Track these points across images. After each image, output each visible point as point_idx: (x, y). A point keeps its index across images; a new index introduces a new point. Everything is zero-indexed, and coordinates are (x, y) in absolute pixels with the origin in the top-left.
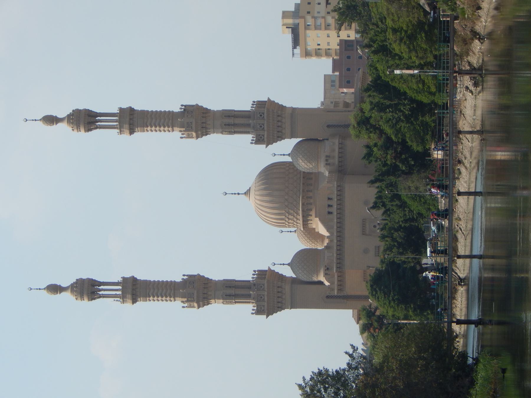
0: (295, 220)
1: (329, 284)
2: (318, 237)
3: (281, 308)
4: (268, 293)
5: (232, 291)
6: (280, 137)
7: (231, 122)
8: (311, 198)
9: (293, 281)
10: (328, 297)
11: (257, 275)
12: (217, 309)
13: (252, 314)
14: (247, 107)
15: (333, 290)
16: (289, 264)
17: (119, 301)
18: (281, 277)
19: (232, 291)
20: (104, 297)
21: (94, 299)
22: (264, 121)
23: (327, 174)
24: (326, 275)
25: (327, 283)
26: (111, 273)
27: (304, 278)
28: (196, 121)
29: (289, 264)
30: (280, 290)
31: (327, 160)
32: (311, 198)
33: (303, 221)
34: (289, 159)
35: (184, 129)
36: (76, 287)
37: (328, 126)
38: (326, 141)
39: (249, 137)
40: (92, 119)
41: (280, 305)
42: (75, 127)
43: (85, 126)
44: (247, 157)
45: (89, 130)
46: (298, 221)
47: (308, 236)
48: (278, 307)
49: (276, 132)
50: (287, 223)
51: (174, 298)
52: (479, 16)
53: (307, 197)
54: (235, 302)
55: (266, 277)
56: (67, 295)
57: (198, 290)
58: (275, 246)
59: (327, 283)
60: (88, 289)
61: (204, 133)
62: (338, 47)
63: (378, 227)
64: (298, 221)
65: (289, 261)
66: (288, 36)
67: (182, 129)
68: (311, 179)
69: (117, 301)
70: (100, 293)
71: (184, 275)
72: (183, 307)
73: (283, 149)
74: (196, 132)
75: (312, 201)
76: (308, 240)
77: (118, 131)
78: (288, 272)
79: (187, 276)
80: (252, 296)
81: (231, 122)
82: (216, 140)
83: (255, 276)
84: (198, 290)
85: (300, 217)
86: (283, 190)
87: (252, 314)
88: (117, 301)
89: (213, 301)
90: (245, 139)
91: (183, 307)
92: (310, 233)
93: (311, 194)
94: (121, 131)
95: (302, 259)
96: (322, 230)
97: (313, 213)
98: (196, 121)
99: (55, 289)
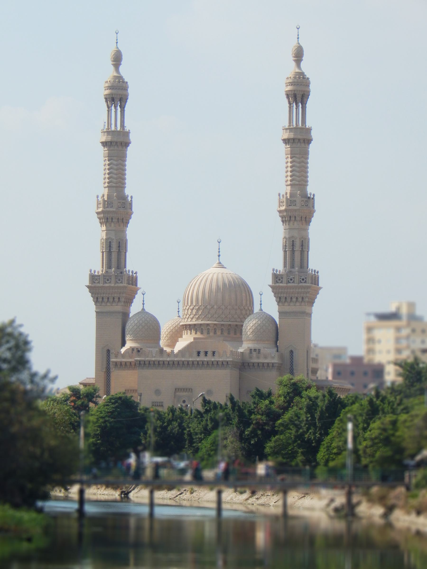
0: (191, 316)
1: (122, 353)
3: (96, 301)
4: (113, 288)
5: (115, 250)
6: (280, 300)
7: (297, 249)
8: (215, 333)
9: (125, 315)
10: (108, 351)
11: (132, 275)
12: (98, 233)
13: (91, 271)
15: (116, 357)
16: (143, 309)
17: (104, 128)
18: (129, 301)
19: (115, 250)
20: (108, 111)
21: (106, 101)
22: (297, 284)
23: (241, 350)
24: (133, 349)
25: (123, 350)
27: (129, 326)
28: (298, 211)
29: (143, 309)
30: (116, 300)
31: (255, 350)
32: (215, 333)
33: (190, 325)
34: (256, 309)
35: (289, 197)
36: (119, 82)
37: (292, 352)
38: (275, 349)
40: (299, 99)
41: (100, 300)
42: (290, 81)
43: (292, 90)
44: (258, 265)
45: (288, 96)
46: (189, 320)
47: (174, 330)
48: (97, 298)
49: (285, 295)
50: (187, 308)
51: (108, 187)
53: (215, 329)
54: (103, 252)
57: (116, 213)
58: (166, 297)
59: (123, 350)
61: (284, 219)
64: (189, 320)
67: (288, 196)
68: (235, 333)
69: (105, 126)
70: (113, 108)
71: (132, 197)
72: (98, 197)
73: (267, 304)
74: (286, 210)
75: (212, 334)
76: (169, 330)
77: (287, 127)
78: (135, 309)
79: (131, 200)
80: (109, 270)
81: (297, 249)
82: (277, 232)
83: (131, 274)
84: (116, 213)
85: (194, 322)
87: (91, 271)
88: (105, 126)
89: (104, 228)
91: (98, 197)
93: (219, 333)
94: (286, 129)
95: (150, 328)
97: (199, 335)
98: (298, 211)
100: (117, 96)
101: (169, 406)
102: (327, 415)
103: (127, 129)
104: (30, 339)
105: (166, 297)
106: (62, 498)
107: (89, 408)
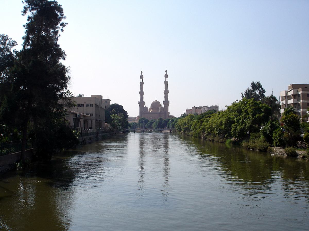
2: (150, 110)
3: (164, 105)
4: (142, 103)
5: (142, 98)
7: (166, 97)
12: (139, 96)
14: (168, 100)
19: (142, 98)
22: (166, 102)
26: (169, 80)
27: (144, 109)
28: (166, 92)
34: (161, 106)
39: (140, 101)
44: (161, 100)
57: (142, 93)
58: (148, 105)
63: (171, 149)
66: (23, 9)
73: (162, 105)
78: (145, 106)
81: (166, 97)
82: (163, 95)
84: (142, 93)
86: (156, 104)
90: (164, 99)
92: (150, 109)
95: (146, 108)
96: (151, 111)
98: (166, 92)
99: (166, 71)
100: (142, 77)
101: (217, 107)
102: (52, 131)
104: (63, 9)
105: (148, 105)
106: (137, 122)
107: (139, 121)
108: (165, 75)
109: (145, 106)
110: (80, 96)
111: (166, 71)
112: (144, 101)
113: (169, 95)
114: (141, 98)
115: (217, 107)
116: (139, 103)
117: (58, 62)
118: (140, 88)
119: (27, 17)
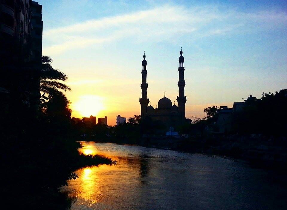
4: (144, 101)
5: (144, 93)
7: (182, 91)
12: (140, 90)
19: (144, 93)
22: (182, 99)
26: (148, 68)
28: (181, 84)
39: (141, 98)
52: (84, 199)
55: (147, 101)
56: (143, 59)
57: (144, 86)
58: (154, 103)
60: (144, 63)
62: (275, 94)
65: (151, 105)
78: (149, 105)
81: (182, 91)
84: (144, 86)
86: (164, 102)
95: (151, 107)
98: (181, 84)
99: (144, 56)
103: (146, 70)
105: (154, 103)
108: (142, 62)
109: (149, 105)
110: (235, 104)
111: (144, 56)
112: (147, 97)
113: (148, 90)
114: (145, 93)
115: (227, 107)
116: (141, 101)
117: (88, 202)
118: (184, 73)
119: (84, 117)
